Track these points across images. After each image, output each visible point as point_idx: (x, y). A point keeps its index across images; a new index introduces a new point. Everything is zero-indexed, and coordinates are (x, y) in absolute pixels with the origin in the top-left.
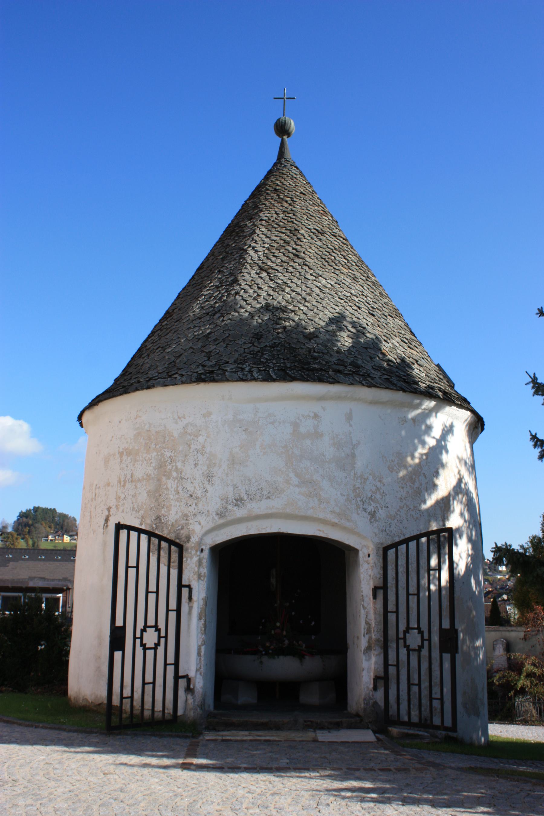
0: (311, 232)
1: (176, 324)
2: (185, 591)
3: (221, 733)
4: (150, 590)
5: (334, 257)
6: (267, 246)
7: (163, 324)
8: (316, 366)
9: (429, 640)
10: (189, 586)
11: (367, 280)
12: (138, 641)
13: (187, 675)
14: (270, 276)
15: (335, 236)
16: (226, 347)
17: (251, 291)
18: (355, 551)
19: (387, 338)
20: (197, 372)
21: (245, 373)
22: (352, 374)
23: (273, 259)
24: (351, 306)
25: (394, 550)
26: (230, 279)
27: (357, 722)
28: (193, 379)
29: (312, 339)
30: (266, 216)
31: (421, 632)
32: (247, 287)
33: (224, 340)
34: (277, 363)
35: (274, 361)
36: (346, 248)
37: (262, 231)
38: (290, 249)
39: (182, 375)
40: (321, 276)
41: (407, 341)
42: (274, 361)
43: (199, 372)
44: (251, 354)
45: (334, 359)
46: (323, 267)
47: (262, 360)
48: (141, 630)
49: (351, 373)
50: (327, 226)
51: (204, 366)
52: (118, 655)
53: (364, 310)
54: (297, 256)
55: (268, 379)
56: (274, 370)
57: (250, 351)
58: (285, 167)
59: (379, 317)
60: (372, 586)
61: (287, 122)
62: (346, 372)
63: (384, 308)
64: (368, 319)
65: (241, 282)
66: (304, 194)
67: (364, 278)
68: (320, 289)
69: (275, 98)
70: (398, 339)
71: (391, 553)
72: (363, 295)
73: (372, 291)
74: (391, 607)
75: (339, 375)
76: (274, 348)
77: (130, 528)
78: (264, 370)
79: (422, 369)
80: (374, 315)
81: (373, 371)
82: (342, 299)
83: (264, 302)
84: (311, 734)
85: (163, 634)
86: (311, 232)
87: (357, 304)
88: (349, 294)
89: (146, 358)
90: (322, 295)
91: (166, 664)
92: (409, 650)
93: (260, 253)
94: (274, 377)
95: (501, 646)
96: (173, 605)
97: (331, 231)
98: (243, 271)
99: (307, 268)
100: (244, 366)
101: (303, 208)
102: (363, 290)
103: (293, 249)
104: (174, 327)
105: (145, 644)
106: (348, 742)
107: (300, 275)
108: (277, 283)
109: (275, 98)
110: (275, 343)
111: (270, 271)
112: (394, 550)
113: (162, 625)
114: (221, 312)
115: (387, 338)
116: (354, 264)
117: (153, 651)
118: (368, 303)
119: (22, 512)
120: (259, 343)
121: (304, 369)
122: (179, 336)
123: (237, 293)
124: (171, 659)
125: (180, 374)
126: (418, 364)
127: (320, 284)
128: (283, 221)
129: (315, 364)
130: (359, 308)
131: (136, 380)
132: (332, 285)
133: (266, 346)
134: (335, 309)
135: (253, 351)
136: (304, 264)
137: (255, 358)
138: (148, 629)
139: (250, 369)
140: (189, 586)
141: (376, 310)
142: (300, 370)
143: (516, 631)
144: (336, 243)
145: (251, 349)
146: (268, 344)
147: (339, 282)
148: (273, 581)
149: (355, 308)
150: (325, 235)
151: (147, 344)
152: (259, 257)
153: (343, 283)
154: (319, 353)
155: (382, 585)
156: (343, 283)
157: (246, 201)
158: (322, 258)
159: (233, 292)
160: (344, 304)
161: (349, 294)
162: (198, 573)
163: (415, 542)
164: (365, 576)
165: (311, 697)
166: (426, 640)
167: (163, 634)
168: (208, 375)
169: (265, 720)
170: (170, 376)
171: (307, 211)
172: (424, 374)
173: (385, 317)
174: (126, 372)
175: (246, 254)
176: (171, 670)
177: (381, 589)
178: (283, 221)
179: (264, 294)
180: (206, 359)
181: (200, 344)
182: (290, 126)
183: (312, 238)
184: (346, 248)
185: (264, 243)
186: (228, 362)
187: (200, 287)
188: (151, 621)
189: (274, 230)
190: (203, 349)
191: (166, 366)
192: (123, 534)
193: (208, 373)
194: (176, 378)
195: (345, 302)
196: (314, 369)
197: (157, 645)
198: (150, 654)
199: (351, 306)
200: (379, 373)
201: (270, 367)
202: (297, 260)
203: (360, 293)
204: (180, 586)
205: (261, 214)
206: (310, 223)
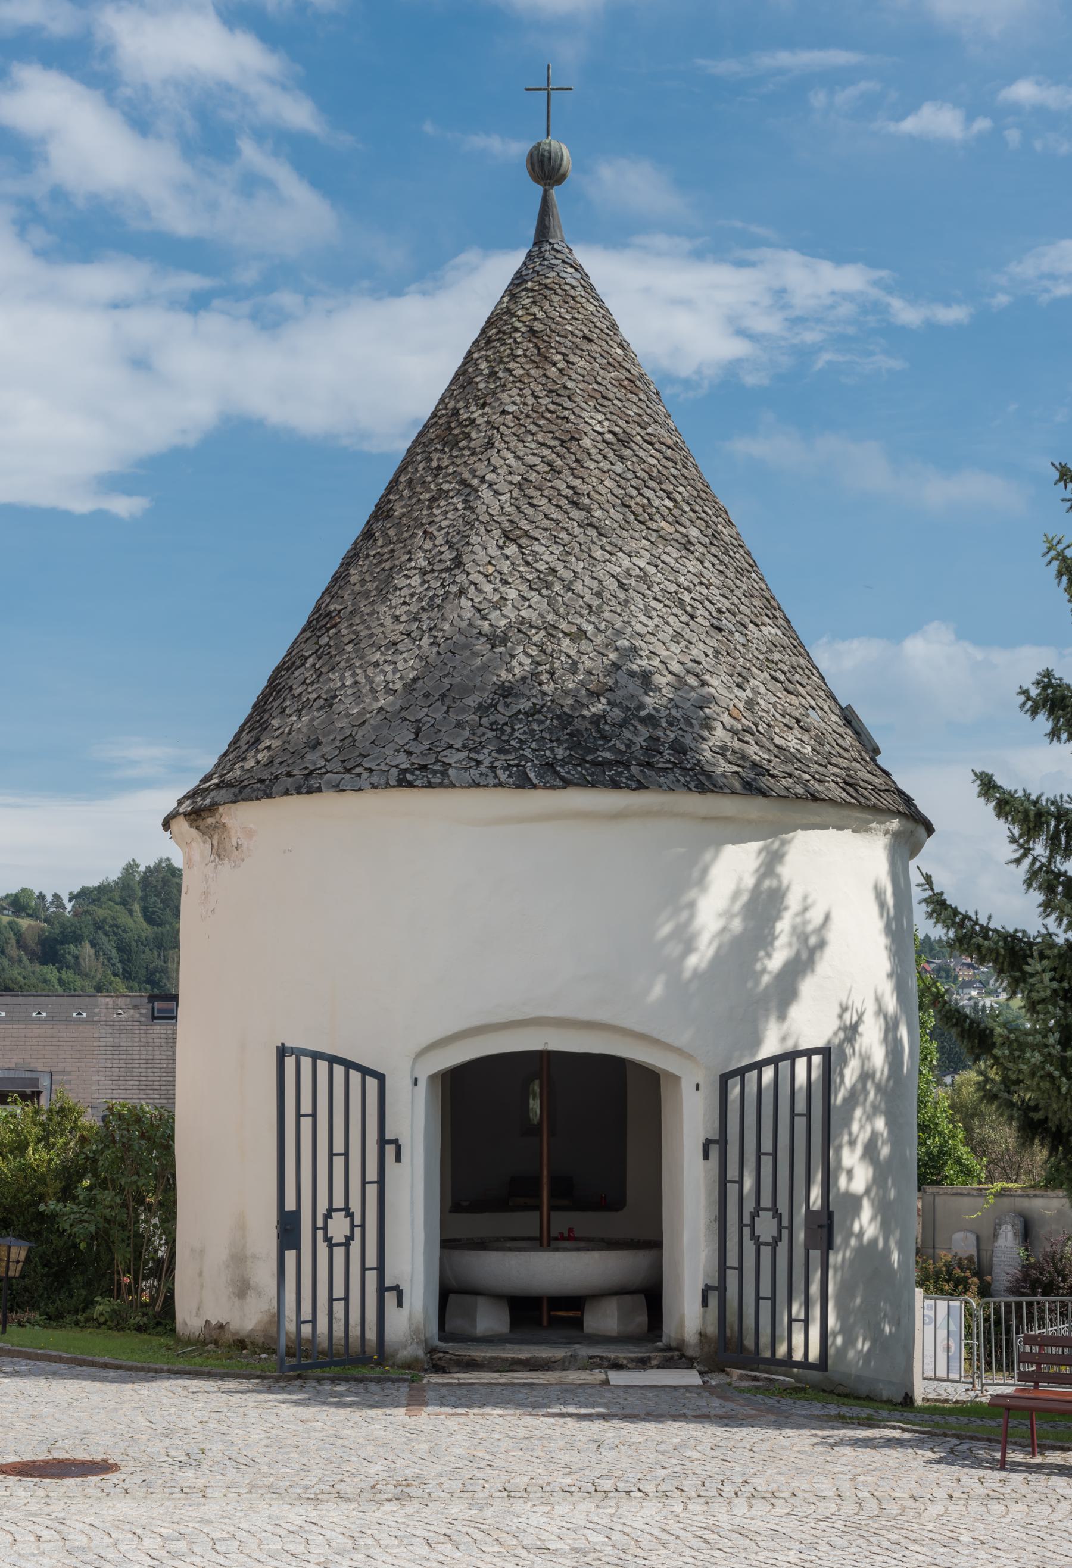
0: (604, 441)
2: (390, 1149)
3: (455, 1375)
4: (334, 1152)
5: (648, 499)
6: (517, 479)
8: (608, 755)
10: (395, 1142)
11: (712, 544)
14: (523, 554)
15: (651, 444)
16: (447, 712)
17: (488, 588)
18: (676, 1079)
20: (397, 766)
23: (530, 511)
24: (676, 616)
27: (676, 1357)
28: (393, 782)
30: (514, 403)
31: (778, 1216)
32: (480, 579)
33: (443, 696)
36: (672, 470)
37: (506, 442)
38: (562, 486)
39: (371, 770)
40: (621, 550)
42: (534, 746)
43: (401, 766)
44: (492, 730)
46: (627, 527)
49: (670, 766)
50: (636, 418)
51: (409, 753)
52: (290, 1255)
54: (575, 504)
55: (523, 783)
56: (534, 766)
58: (551, 267)
61: (553, 155)
62: (661, 765)
63: (742, 607)
65: (470, 567)
66: (590, 340)
68: (618, 581)
69: (527, 90)
72: (701, 583)
73: (721, 568)
76: (532, 715)
77: (299, 1053)
78: (517, 765)
80: (720, 630)
82: (660, 602)
83: (513, 615)
84: (598, 1375)
85: (358, 1221)
86: (604, 441)
88: (673, 588)
90: (622, 595)
91: (364, 1269)
93: (503, 498)
94: (535, 781)
95: (1009, 1227)
96: (372, 1174)
97: (643, 433)
98: (472, 541)
99: (593, 533)
100: (480, 757)
101: (587, 378)
103: (569, 487)
105: (331, 1238)
107: (582, 551)
108: (537, 570)
109: (527, 90)
111: (524, 541)
113: (355, 1206)
117: (343, 1248)
118: (710, 602)
120: (507, 705)
121: (587, 762)
123: (462, 592)
124: (372, 1261)
125: (366, 769)
126: (801, 727)
127: (618, 570)
128: (548, 415)
129: (604, 750)
130: (692, 617)
132: (641, 569)
133: (519, 711)
134: (646, 626)
135: (495, 723)
136: (588, 525)
137: (499, 738)
138: (770, 1240)
139: (492, 763)
140: (395, 1142)
141: (727, 614)
142: (579, 765)
143: (1043, 1196)
147: (654, 560)
148: (535, 1105)
152: (502, 508)
153: (663, 562)
155: (717, 1138)
156: (663, 562)
158: (624, 505)
160: (664, 610)
161: (673, 588)
162: (414, 1118)
163: (772, 1067)
165: (604, 1319)
166: (784, 1227)
167: (358, 1221)
169: (523, 1356)
170: (349, 771)
171: (596, 387)
172: (809, 748)
173: (742, 628)
175: (475, 499)
176: (372, 1277)
177: (715, 1146)
178: (548, 415)
179: (512, 594)
180: (412, 736)
182: (561, 165)
183: (605, 457)
185: (510, 473)
188: (339, 1202)
189: (529, 438)
190: (404, 714)
191: (338, 744)
192: (290, 1062)
193: (416, 769)
194: (359, 775)
195: (665, 606)
196: (604, 764)
197: (350, 1238)
199: (676, 616)
201: (527, 760)
202: (575, 514)
203: (696, 581)
204: (382, 1142)
205: (504, 397)
206: (600, 417)
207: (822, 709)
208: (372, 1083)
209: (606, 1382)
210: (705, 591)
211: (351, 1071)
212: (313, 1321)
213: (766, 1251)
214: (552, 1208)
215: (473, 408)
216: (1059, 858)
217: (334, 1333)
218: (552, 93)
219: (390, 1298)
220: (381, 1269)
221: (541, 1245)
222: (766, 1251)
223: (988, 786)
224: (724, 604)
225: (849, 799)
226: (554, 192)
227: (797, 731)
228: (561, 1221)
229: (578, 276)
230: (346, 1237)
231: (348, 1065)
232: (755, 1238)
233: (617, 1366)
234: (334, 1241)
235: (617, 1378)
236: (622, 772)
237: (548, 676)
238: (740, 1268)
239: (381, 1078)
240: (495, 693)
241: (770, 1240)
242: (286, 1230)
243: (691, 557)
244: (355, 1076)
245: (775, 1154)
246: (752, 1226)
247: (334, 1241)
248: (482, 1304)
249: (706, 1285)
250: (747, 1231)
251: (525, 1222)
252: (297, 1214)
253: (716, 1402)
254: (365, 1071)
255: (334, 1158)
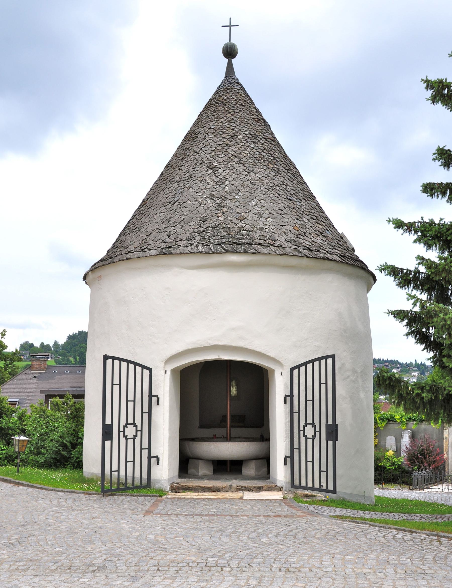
1: (148, 210)
2: (154, 400)
3: (179, 494)
7: (140, 210)
9: (320, 432)
12: (122, 434)
13: (157, 456)
19: (300, 217)
20: (160, 247)
21: (193, 247)
22: (269, 246)
25: (297, 369)
26: (186, 176)
29: (242, 220)
31: (314, 426)
34: (216, 240)
35: (214, 238)
36: (273, 148)
41: (315, 218)
45: (257, 235)
47: (206, 237)
48: (124, 426)
49: (269, 245)
50: (260, 131)
51: (165, 242)
52: (108, 443)
53: (283, 196)
57: (198, 231)
59: (294, 201)
60: (283, 396)
62: (265, 245)
64: (285, 203)
67: (286, 171)
70: (308, 217)
71: (296, 372)
72: (284, 184)
74: (296, 409)
75: (259, 247)
77: (113, 358)
78: (207, 245)
79: (325, 239)
81: (285, 243)
84: (240, 494)
87: (278, 192)
89: (127, 236)
92: (307, 439)
95: (407, 435)
96: (146, 409)
97: (262, 135)
100: (192, 243)
102: (284, 181)
104: (147, 212)
106: (263, 500)
110: (216, 224)
112: (297, 369)
113: (138, 423)
114: (179, 201)
115: (300, 217)
116: (279, 160)
118: (287, 191)
119: (70, 335)
122: (150, 219)
124: (145, 445)
131: (120, 253)
138: (128, 426)
139: (197, 245)
142: (232, 245)
144: (265, 144)
145: (199, 229)
146: (210, 225)
149: (277, 195)
150: (258, 138)
151: (129, 225)
154: (246, 231)
157: (201, 112)
159: (188, 186)
162: (165, 388)
164: (279, 387)
166: (317, 432)
167: (139, 429)
168: (167, 249)
170: (142, 250)
174: (115, 246)
176: (145, 452)
177: (289, 398)
181: (164, 226)
184: (273, 148)
186: (182, 240)
187: (165, 182)
190: (166, 230)
191: (140, 242)
192: (109, 362)
198: (130, 442)
200: (290, 244)
204: (151, 396)
207: (331, 231)
208: (146, 372)
209: (242, 498)
210: (285, 187)
211: (144, 370)
212: (118, 471)
213: (310, 441)
214: (231, 426)
215: (200, 129)
216: (424, 297)
217: (135, 476)
218: (232, 25)
219: (153, 461)
220: (149, 449)
221: (227, 440)
222: (310, 441)
223: (399, 224)
224: (292, 192)
225: (342, 261)
226: (233, 60)
227: (321, 237)
228: (236, 432)
229: (240, 86)
230: (134, 435)
231: (136, 364)
232: (305, 436)
233: (248, 489)
234: (128, 437)
235: (248, 496)
236: (249, 247)
237: (222, 214)
238: (299, 449)
239: (150, 370)
240: (200, 220)
241: (128, 426)
242: (106, 432)
243: (280, 176)
244: (139, 369)
245: (313, 401)
246: (304, 431)
247: (128, 437)
248: (201, 463)
249: (286, 456)
250: (302, 433)
251: (220, 432)
252: (111, 426)
253: (286, 508)
254: (143, 367)
255: (129, 402)
